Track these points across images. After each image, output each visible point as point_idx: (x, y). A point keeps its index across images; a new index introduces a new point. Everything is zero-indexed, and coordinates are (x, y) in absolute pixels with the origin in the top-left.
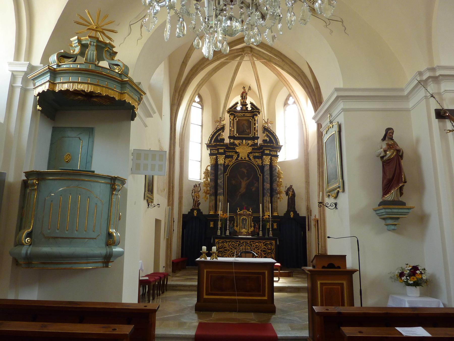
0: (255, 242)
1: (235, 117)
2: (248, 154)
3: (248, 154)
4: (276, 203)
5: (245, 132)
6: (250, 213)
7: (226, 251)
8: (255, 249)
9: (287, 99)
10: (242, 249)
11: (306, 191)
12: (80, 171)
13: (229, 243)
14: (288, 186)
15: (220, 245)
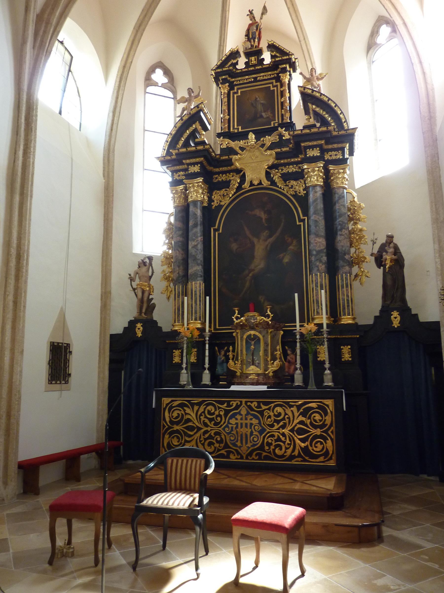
0: (273, 405)
1: (232, 87)
2: (268, 170)
3: (268, 170)
4: (347, 290)
5: (260, 120)
6: (268, 320)
7: (192, 430)
8: (272, 426)
9: (374, 33)
10: (235, 426)
11: (437, 246)
13: (199, 409)
14: (382, 240)
15: (175, 414)
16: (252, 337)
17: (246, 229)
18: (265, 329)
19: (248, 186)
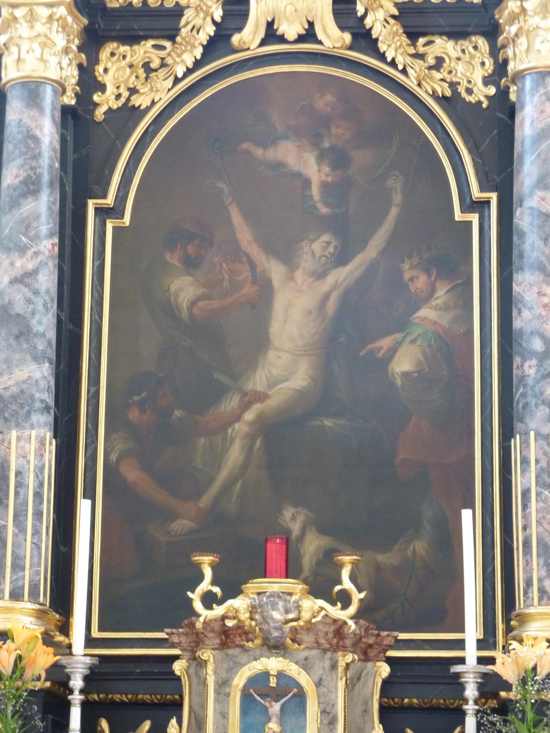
12: (161, 675)
16: (273, 682)
17: (236, 218)
18: (325, 651)
19: (258, 41)
